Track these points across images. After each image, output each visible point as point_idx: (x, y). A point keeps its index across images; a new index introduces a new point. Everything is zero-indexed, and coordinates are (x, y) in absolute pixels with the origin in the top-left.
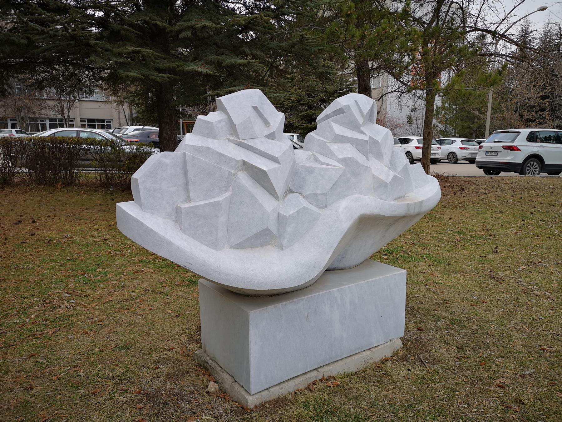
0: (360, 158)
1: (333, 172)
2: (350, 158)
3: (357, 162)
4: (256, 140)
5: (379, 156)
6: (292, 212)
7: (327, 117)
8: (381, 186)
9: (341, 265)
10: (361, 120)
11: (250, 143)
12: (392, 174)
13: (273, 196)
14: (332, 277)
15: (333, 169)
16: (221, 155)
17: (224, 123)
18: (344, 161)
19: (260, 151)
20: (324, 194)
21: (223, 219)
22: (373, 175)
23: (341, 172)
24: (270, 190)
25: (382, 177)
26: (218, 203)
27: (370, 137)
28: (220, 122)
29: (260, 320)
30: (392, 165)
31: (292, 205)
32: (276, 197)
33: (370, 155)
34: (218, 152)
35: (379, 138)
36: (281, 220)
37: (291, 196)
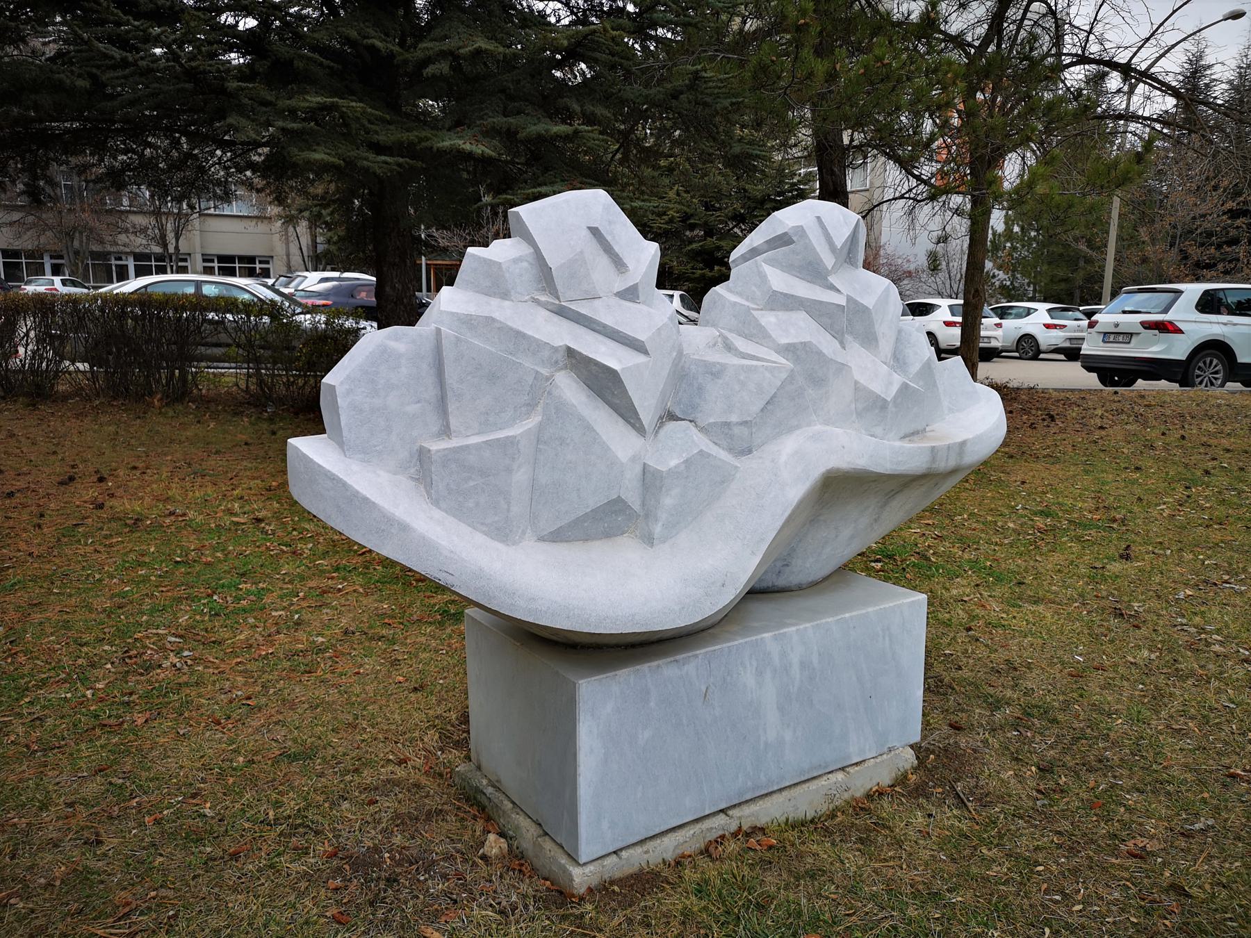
0: (827, 344)
1: (768, 375)
2: (804, 344)
3: (820, 353)
4: (597, 302)
5: (869, 339)
6: (673, 463)
7: (754, 252)
8: (873, 408)
9: (781, 582)
10: (828, 260)
11: (583, 309)
12: (898, 380)
13: (633, 426)
14: (764, 608)
15: (766, 368)
16: (519, 335)
17: (525, 264)
18: (789, 350)
19: (605, 326)
20: (745, 423)
21: (521, 476)
22: (856, 382)
23: (784, 376)
24: (627, 413)
25: (877, 387)
26: (510, 442)
27: (849, 299)
28: (516, 261)
29: (600, 701)
30: (898, 361)
31: (676, 447)
32: (639, 429)
33: (848, 338)
34: (511, 329)
35: (869, 301)
36: (650, 480)
37: (671, 426)
